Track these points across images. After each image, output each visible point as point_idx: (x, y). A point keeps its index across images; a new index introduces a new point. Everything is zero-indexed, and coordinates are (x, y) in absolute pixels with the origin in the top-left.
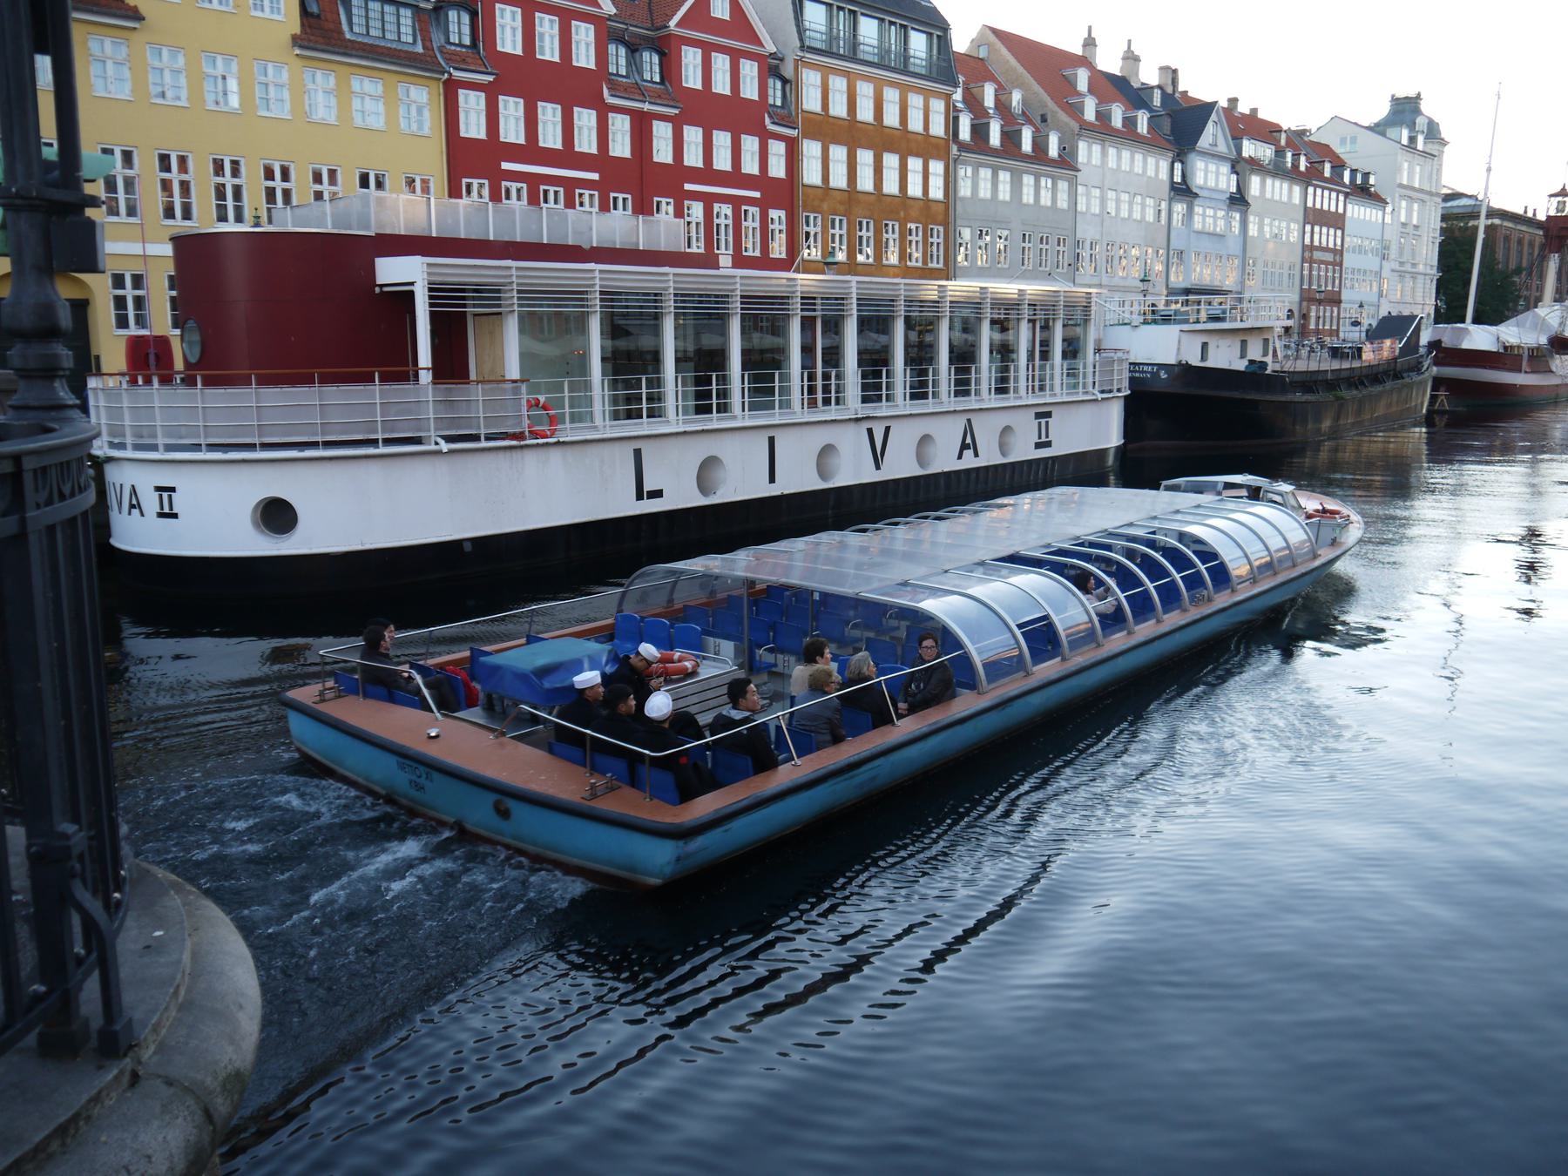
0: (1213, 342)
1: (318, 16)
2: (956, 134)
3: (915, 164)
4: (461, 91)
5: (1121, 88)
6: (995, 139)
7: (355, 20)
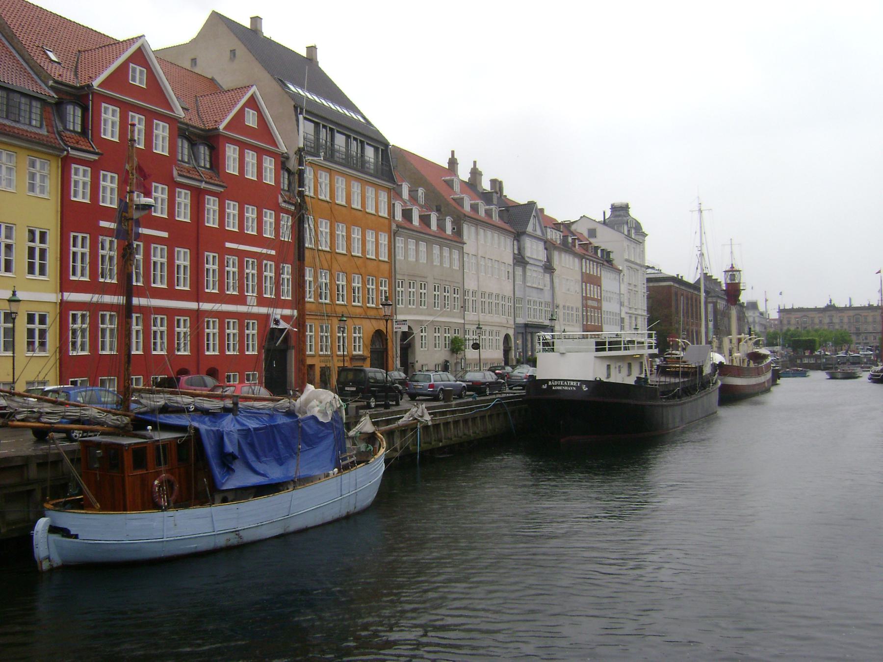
3: (370, 237)
4: (74, 166)
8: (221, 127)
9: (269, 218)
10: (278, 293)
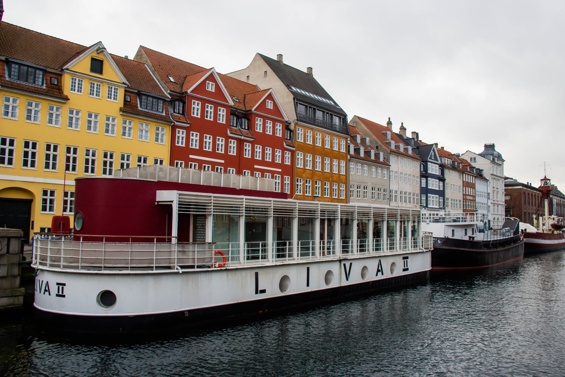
0: (456, 230)
1: (130, 102)
2: (349, 152)
3: (335, 163)
4: (177, 129)
5: (400, 137)
6: (362, 155)
7: (143, 103)
8: (253, 109)
9: (278, 153)
10: (305, 192)
